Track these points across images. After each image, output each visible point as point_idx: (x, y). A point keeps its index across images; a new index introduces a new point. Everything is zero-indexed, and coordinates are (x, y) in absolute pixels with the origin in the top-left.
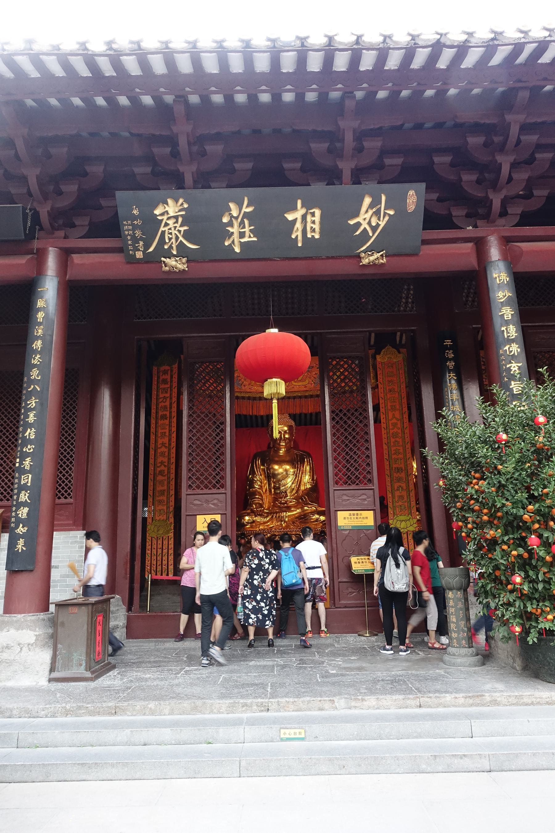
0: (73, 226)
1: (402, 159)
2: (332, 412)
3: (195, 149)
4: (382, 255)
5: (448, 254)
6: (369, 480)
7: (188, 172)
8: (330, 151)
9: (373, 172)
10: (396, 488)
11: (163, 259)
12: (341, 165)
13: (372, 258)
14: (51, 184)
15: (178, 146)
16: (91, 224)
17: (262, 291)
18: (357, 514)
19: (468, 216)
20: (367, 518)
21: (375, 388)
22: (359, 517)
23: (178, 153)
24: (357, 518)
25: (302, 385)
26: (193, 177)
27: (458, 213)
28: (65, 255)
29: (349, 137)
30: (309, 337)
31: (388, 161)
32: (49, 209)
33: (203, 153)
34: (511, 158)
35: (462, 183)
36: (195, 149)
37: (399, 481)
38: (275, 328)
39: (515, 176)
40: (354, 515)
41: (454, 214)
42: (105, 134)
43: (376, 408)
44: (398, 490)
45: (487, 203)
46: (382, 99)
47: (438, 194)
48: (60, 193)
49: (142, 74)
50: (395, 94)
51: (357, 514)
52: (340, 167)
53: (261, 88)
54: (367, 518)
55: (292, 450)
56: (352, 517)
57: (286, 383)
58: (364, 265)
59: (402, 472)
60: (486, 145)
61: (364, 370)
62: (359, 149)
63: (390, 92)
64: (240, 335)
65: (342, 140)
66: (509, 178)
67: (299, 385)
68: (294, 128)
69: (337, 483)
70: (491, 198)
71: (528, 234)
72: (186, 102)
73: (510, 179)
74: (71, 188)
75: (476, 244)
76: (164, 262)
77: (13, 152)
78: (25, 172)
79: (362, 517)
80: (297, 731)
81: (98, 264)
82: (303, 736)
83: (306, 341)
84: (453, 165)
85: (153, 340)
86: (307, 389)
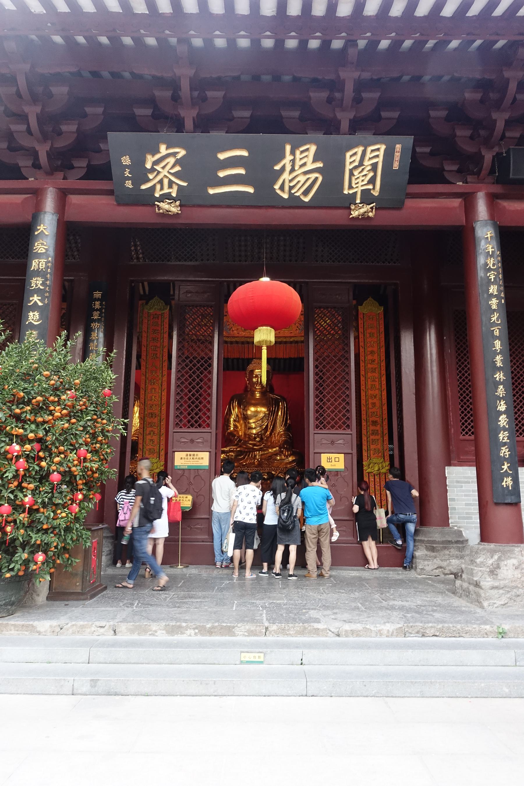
0: (72, 167)
1: (399, 113)
2: (316, 360)
3: (196, 94)
4: (372, 208)
5: (429, 208)
6: (208, 424)
7: (189, 115)
8: (330, 100)
9: (368, 125)
10: (148, 433)
11: (156, 203)
12: (339, 115)
13: (362, 211)
14: (50, 125)
15: (180, 90)
16: (89, 166)
17: (249, 238)
18: (194, 455)
19: (459, 171)
20: (182, 458)
21: (357, 338)
22: (195, 457)
23: (179, 97)
24: (193, 458)
25: (294, 331)
26: (194, 123)
27: (450, 167)
28: (63, 196)
29: (349, 88)
30: (298, 287)
31: (384, 114)
32: (48, 150)
33: (204, 99)
34: (506, 115)
35: (456, 138)
36: (196, 94)
37: (151, 427)
38: (267, 277)
39: (508, 134)
40: (190, 455)
41: (447, 168)
42: (287, 78)
43: (357, 356)
44: (150, 434)
45: (478, 159)
46: (382, 50)
47: (430, 148)
48: (60, 133)
49: (96, 11)
50: (396, 44)
51: (194, 455)
52: (182, 115)
53: (265, 34)
54: (202, 458)
55: (268, 393)
56: (189, 457)
57: (275, 331)
58: (353, 217)
59: (155, 417)
60: (482, 101)
61: (350, 319)
62: (358, 100)
63: (391, 42)
64: (238, 281)
65: (342, 90)
66: (502, 136)
67: (285, 332)
68: (295, 75)
69: (317, 427)
70: (483, 154)
71: (417, 191)
72: (190, 44)
73: (503, 137)
74: (70, 128)
75: (465, 200)
76: (158, 206)
77: (14, 89)
78: (26, 109)
79: (198, 457)
80: (257, 655)
81: (95, 207)
82: (262, 659)
83: (295, 288)
84: (448, 119)
85: (137, 281)
86: (292, 335)
